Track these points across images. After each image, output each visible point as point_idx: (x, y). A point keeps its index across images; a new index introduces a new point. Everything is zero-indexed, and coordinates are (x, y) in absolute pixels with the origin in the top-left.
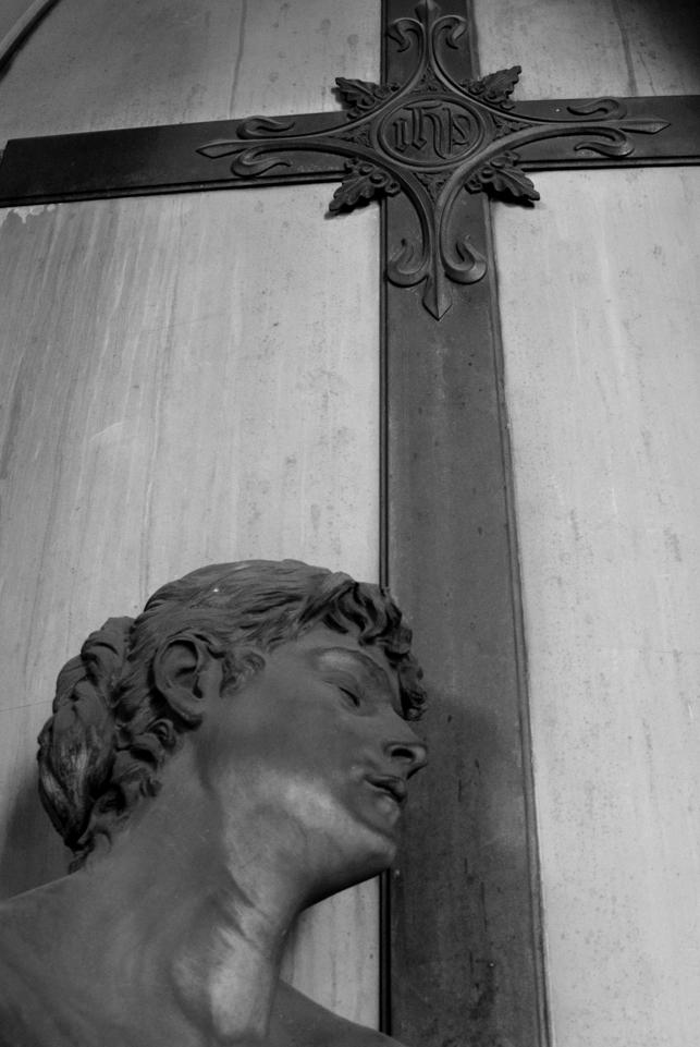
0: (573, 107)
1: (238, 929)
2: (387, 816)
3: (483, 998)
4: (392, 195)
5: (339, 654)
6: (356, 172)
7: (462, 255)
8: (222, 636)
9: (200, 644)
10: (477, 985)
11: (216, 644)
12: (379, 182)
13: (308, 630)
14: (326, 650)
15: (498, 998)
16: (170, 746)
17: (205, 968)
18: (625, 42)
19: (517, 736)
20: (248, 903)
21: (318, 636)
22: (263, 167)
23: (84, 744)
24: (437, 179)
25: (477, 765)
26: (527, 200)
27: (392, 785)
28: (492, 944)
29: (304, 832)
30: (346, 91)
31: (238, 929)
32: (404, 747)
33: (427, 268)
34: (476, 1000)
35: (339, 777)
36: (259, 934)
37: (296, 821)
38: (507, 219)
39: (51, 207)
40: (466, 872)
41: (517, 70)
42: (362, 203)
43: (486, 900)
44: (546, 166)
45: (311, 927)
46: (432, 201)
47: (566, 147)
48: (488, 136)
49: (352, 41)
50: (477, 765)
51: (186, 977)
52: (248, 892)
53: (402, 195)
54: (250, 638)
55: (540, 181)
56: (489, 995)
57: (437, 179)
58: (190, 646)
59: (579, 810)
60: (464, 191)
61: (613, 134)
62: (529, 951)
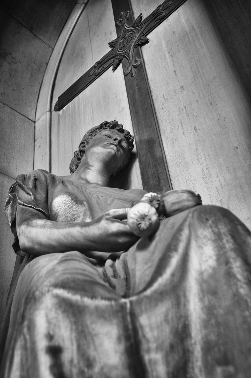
1: (91, 170)
4: (122, 59)
5: (106, 132)
7: (136, 61)
13: (101, 131)
20: (92, 166)
30: (112, 45)
31: (91, 170)
33: (130, 69)
39: (69, 104)
41: (141, 14)
46: (128, 56)
47: (152, 24)
51: (83, 176)
60: (135, 49)
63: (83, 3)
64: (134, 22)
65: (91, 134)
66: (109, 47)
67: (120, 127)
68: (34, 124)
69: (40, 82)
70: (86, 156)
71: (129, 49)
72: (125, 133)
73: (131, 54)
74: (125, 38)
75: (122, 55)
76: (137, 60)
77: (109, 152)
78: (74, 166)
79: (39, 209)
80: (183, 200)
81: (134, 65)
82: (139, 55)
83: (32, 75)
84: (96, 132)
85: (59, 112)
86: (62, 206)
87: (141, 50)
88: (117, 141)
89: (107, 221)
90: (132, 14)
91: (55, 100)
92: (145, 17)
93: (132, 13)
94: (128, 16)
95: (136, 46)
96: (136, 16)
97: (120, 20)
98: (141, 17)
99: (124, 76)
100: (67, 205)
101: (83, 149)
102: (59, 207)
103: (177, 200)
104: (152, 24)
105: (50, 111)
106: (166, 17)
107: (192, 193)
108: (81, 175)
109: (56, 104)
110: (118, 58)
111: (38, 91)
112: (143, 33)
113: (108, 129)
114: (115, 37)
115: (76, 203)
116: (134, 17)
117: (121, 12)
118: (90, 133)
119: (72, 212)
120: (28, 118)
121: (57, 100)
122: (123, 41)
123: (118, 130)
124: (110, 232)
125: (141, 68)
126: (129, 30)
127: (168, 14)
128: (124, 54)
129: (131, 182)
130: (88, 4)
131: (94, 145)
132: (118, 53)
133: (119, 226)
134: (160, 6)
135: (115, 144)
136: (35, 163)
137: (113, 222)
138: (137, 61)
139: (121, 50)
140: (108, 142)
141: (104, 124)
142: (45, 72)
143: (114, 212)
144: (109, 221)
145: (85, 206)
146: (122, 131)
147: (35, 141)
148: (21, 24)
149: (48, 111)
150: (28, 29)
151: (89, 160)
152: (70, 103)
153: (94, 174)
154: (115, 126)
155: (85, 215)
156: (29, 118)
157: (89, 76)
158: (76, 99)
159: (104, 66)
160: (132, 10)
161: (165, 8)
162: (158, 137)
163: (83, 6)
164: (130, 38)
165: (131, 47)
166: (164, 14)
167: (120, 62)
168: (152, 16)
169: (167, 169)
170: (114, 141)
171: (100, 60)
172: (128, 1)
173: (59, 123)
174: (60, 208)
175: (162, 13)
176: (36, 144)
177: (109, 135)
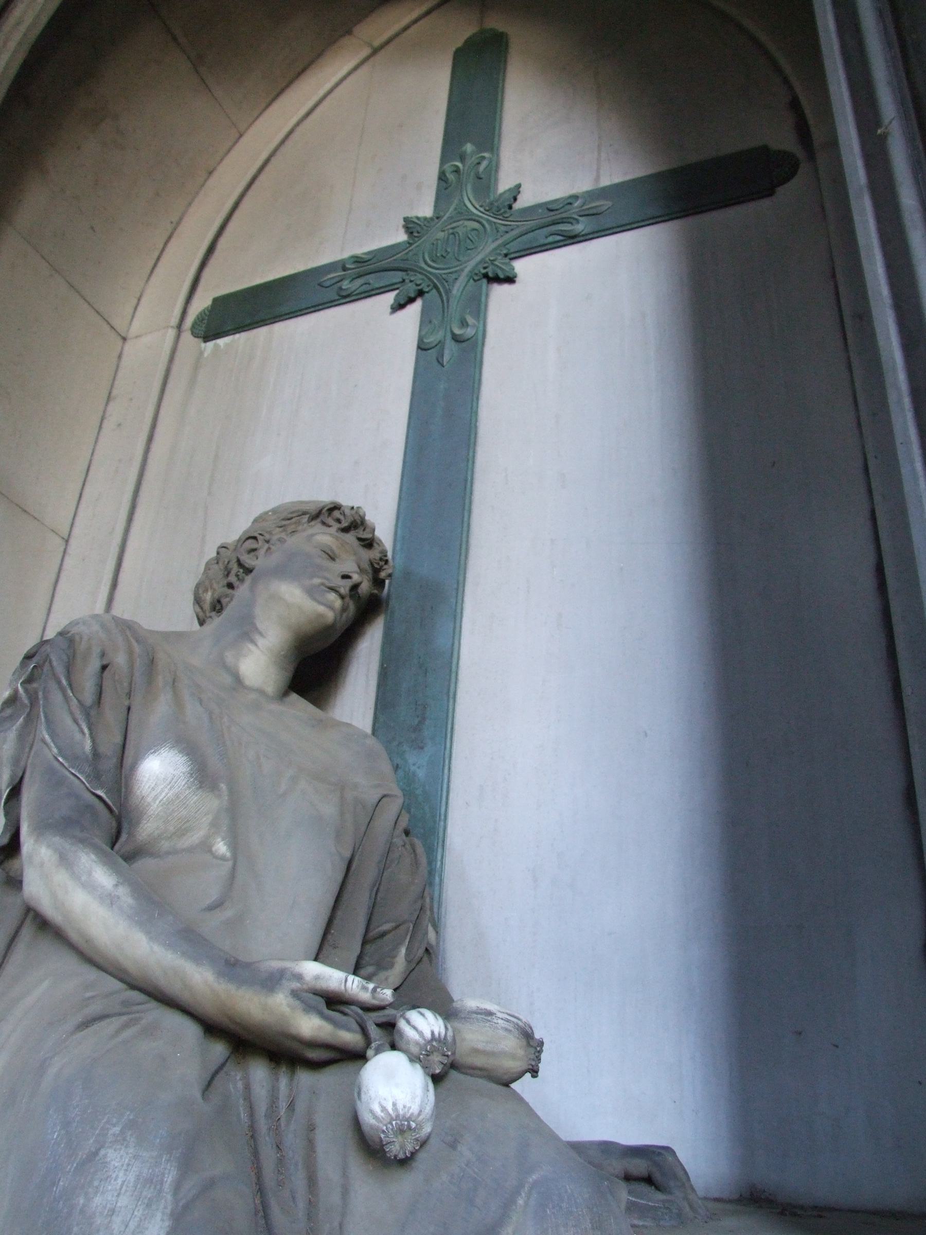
0: (550, 207)
1: (256, 645)
3: (420, 722)
4: (427, 292)
5: (325, 536)
6: (407, 281)
7: (464, 324)
8: (270, 533)
9: (260, 537)
11: (267, 537)
12: (419, 285)
13: (312, 526)
14: (316, 534)
15: (427, 722)
16: (242, 580)
18: (599, 147)
19: (454, 593)
20: (261, 634)
21: (317, 527)
22: (354, 288)
24: (454, 276)
26: (510, 280)
30: (412, 226)
31: (256, 645)
33: (439, 336)
38: (499, 291)
39: (237, 336)
41: (519, 186)
42: (411, 300)
44: (528, 252)
46: (448, 292)
47: (541, 236)
48: (490, 240)
49: (419, 187)
51: (229, 657)
53: (434, 291)
55: (521, 266)
56: (423, 719)
57: (454, 276)
58: (255, 538)
60: (471, 281)
61: (571, 220)
63: (370, 45)
64: (492, 198)
66: (401, 226)
67: (367, 530)
68: (120, 342)
69: (175, 220)
70: (252, 589)
71: (456, 272)
72: (374, 554)
73: (456, 290)
74: (453, 234)
75: (430, 279)
76: (467, 323)
77: (321, 616)
78: (210, 593)
79: (100, 792)
80: (503, 1054)
81: (457, 331)
82: (477, 307)
83: (158, 194)
84: (299, 523)
85: (203, 345)
86: (162, 791)
87: (487, 295)
89: (291, 1000)
90: (494, 168)
91: (202, 302)
92: (525, 200)
93: (494, 163)
94: (482, 168)
95: (476, 274)
96: (504, 184)
97: (457, 166)
98: (516, 191)
99: (419, 347)
100: (176, 790)
101: (248, 561)
102: (153, 789)
103: (489, 1048)
104: (541, 236)
105: (179, 327)
106: (582, 238)
107: (527, 1035)
108: (227, 654)
109: (201, 313)
110: (418, 282)
111: (161, 246)
112: (508, 246)
113: (333, 530)
114: (426, 210)
115: (200, 787)
116: (496, 189)
117: (466, 143)
118: (283, 520)
119: (184, 813)
120: (108, 323)
121: (208, 303)
122: (448, 238)
123: (360, 539)
124: (293, 1031)
125: (470, 348)
126: (474, 214)
127: (593, 233)
128: (437, 278)
129: (345, 677)
130: (383, 52)
131: (281, 572)
132: (423, 265)
133: (320, 1028)
134: (575, 197)
135: (342, 591)
136: (92, 468)
137: (309, 1008)
138: (468, 325)
139: (433, 261)
140: (324, 581)
142: (197, 193)
143: (317, 978)
144: (298, 1002)
145: (219, 796)
146: (369, 543)
147: (109, 398)
148: (175, 39)
149: (172, 327)
150: (189, 58)
151: (258, 611)
152: (243, 334)
153: (258, 665)
154: (356, 525)
155: (214, 824)
156: (113, 323)
157: (320, 285)
158: (262, 332)
159: (371, 278)
160: (498, 155)
161: (586, 213)
162: (457, 589)
163: (366, 52)
164: (468, 241)
165: (462, 270)
166: (579, 228)
167: (421, 293)
168: (546, 211)
170: (340, 579)
171: (365, 254)
173: (193, 381)
174: (154, 794)
175: (578, 222)
176: (109, 408)
177: (332, 550)
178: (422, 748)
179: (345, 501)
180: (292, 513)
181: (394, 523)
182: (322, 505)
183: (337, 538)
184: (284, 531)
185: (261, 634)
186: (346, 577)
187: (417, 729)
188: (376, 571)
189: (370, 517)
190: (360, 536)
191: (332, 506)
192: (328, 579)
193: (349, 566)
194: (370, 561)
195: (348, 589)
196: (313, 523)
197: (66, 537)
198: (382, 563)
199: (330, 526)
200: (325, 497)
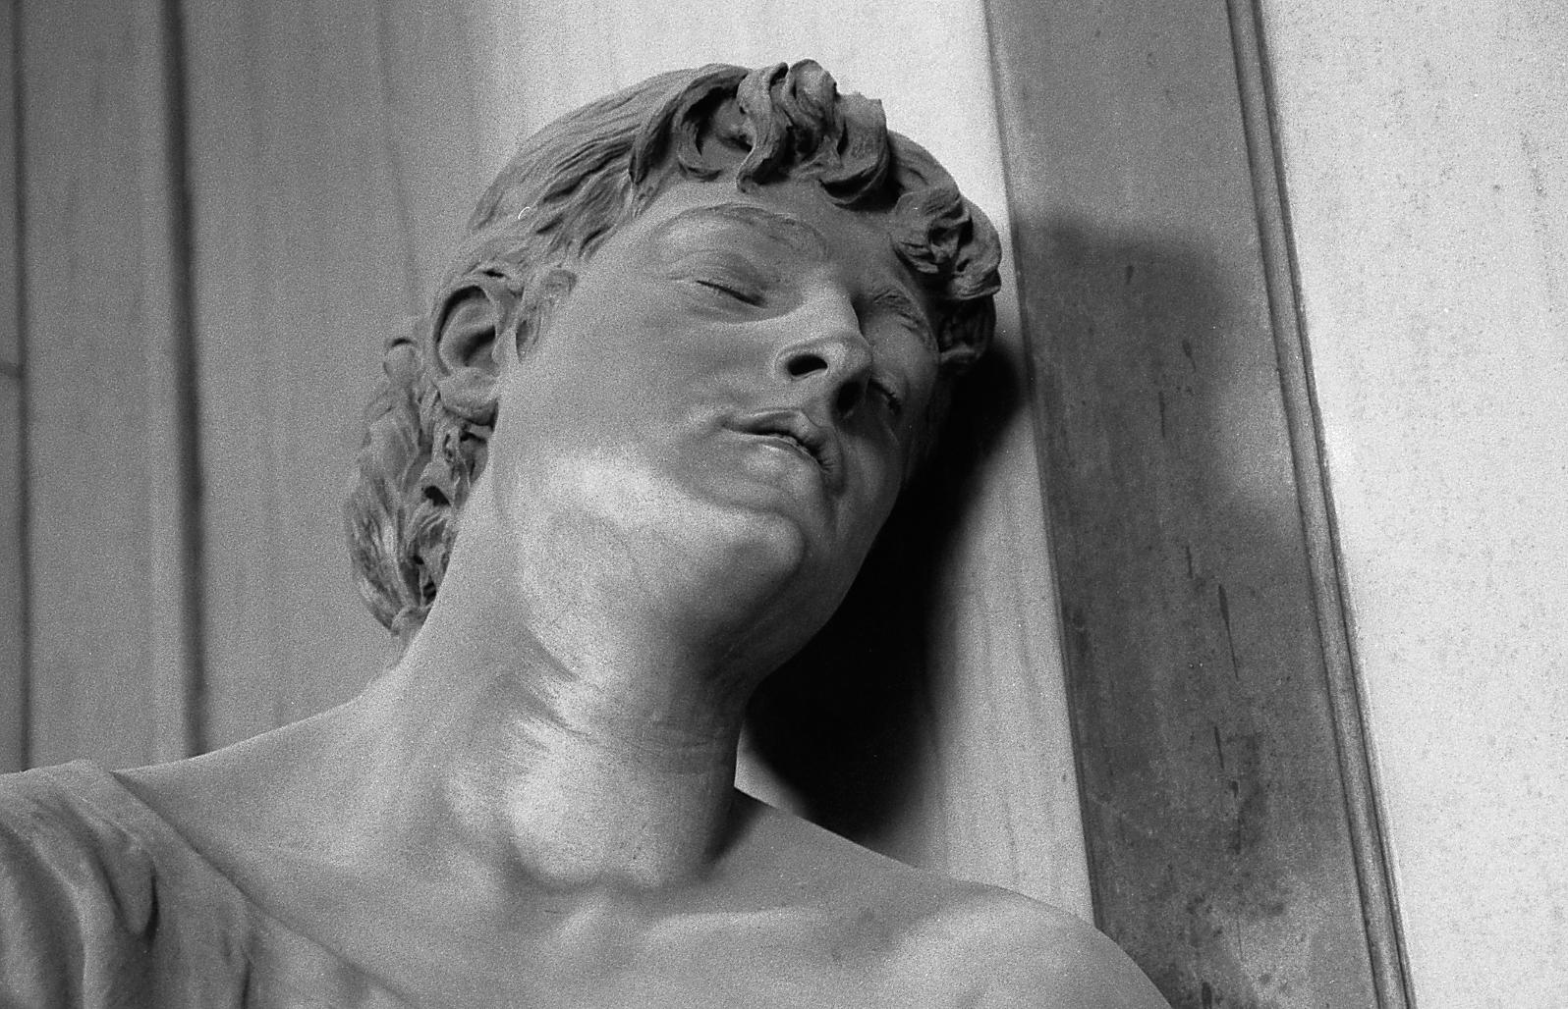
1: (552, 717)
2: (777, 480)
3: (1247, 805)
5: (686, 222)
10: (1234, 787)
15: (1272, 801)
17: (499, 775)
20: (561, 672)
23: (382, 511)
25: (1187, 349)
27: (783, 424)
28: (1250, 701)
29: (619, 539)
31: (552, 717)
32: (804, 351)
34: (1235, 814)
35: (665, 434)
36: (595, 721)
37: (609, 526)
40: (1190, 572)
43: (1231, 615)
45: (963, 748)
50: (1187, 349)
52: (566, 660)
54: (554, 248)
59: (1402, 384)
62: (1318, 698)
65: (551, 212)
67: (855, 140)
72: (908, 223)
78: (389, 532)
88: (818, 383)
113: (726, 192)
123: (835, 189)
135: (802, 425)
140: (727, 408)
141: (688, 116)
169: (1338, 672)
172: (113, 998)
178: (1279, 909)
179: (750, 50)
180: (572, 163)
181: (981, 41)
182: (661, 103)
183: (744, 215)
184: (565, 241)
185: (561, 672)
186: (803, 364)
187: (1243, 837)
188: (936, 286)
189: (858, 80)
190: (831, 177)
191: (700, 94)
192: (742, 399)
193: (816, 317)
194: (900, 255)
195: (823, 409)
196: (652, 181)
197: (10, 355)
198: (949, 247)
199: (712, 176)
200: (685, 54)
